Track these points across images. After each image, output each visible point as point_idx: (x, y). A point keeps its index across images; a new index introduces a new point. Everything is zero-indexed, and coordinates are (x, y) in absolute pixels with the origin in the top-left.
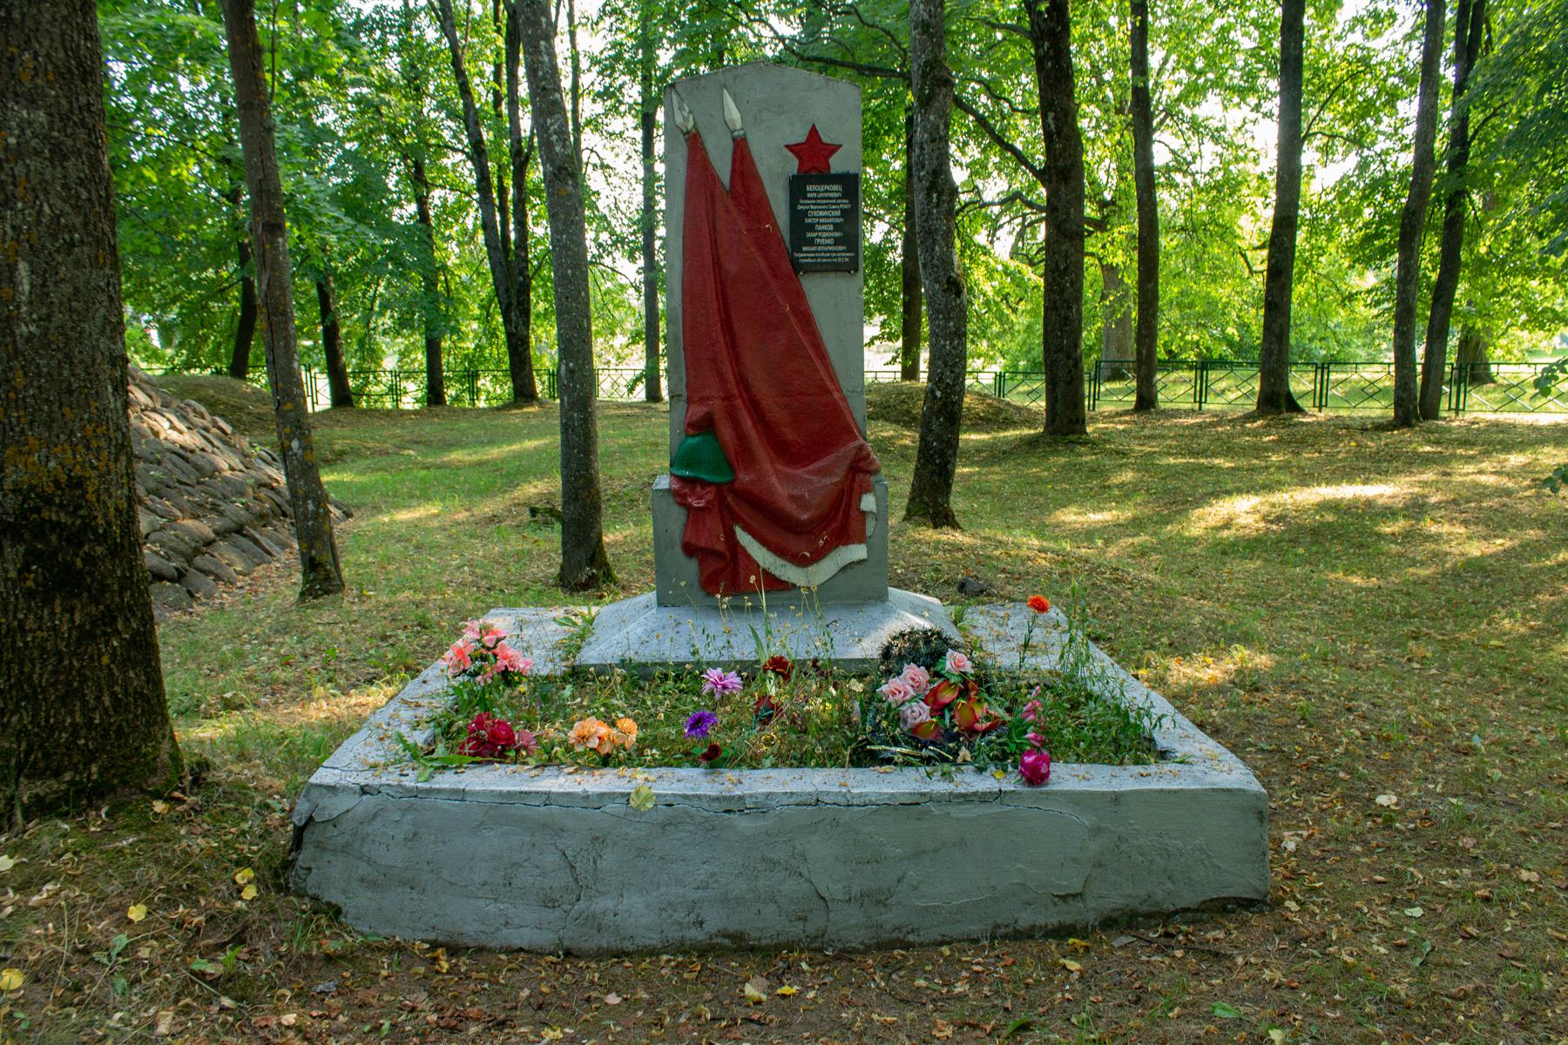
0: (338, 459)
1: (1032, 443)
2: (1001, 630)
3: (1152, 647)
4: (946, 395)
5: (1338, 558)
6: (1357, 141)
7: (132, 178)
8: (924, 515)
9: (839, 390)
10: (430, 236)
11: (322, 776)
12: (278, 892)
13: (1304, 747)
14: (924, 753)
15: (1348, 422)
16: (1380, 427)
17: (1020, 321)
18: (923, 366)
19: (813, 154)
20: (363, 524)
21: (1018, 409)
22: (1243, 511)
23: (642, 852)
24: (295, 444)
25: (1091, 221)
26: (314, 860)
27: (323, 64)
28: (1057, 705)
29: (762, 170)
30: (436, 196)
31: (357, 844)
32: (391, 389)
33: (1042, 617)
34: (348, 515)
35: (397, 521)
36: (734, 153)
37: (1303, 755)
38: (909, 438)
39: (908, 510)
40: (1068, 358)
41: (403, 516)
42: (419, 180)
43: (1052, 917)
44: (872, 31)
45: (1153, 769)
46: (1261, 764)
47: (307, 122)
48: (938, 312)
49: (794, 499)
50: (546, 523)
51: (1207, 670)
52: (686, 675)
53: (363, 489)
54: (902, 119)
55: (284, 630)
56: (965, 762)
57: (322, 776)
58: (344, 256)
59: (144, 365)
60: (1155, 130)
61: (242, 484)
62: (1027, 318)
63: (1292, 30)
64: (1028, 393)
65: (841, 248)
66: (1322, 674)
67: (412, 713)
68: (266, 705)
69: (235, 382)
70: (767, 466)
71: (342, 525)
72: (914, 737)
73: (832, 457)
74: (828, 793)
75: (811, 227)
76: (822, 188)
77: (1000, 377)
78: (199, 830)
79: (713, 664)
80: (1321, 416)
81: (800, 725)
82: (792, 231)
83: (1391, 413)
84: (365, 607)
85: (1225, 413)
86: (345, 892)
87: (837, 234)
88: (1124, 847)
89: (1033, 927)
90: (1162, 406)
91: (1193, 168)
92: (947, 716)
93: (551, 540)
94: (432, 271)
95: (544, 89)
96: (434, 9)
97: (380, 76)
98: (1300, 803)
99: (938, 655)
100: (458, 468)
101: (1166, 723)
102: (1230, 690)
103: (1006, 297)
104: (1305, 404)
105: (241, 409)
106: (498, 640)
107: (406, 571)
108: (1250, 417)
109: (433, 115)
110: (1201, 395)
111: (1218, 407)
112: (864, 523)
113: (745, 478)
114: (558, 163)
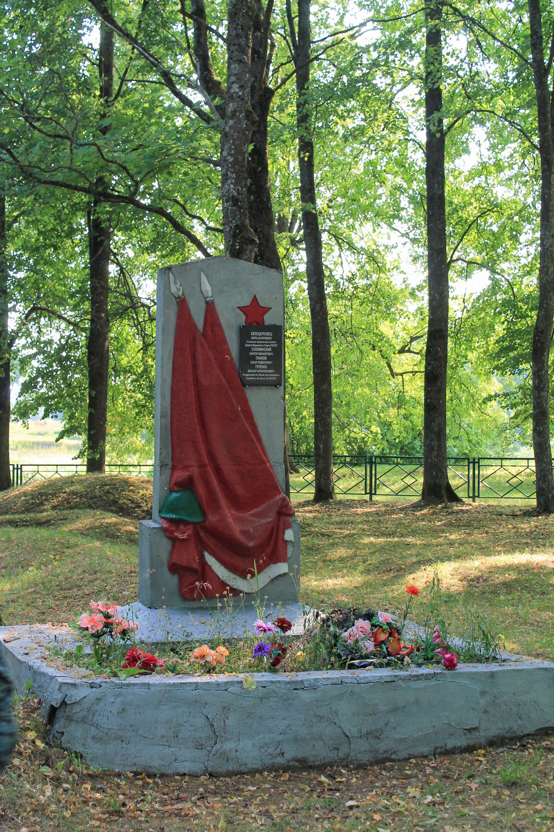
6: (490, 265)
9: (269, 462)
15: (499, 509)
16: (528, 514)
23: (249, 715)
31: (90, 716)
43: (462, 742)
49: (243, 532)
65: (271, 371)
73: (266, 505)
74: (347, 677)
76: (260, 334)
83: (534, 502)
86: (84, 745)
87: (269, 363)
88: (497, 701)
89: (454, 748)
92: (384, 647)
108: (416, 507)
113: (212, 519)
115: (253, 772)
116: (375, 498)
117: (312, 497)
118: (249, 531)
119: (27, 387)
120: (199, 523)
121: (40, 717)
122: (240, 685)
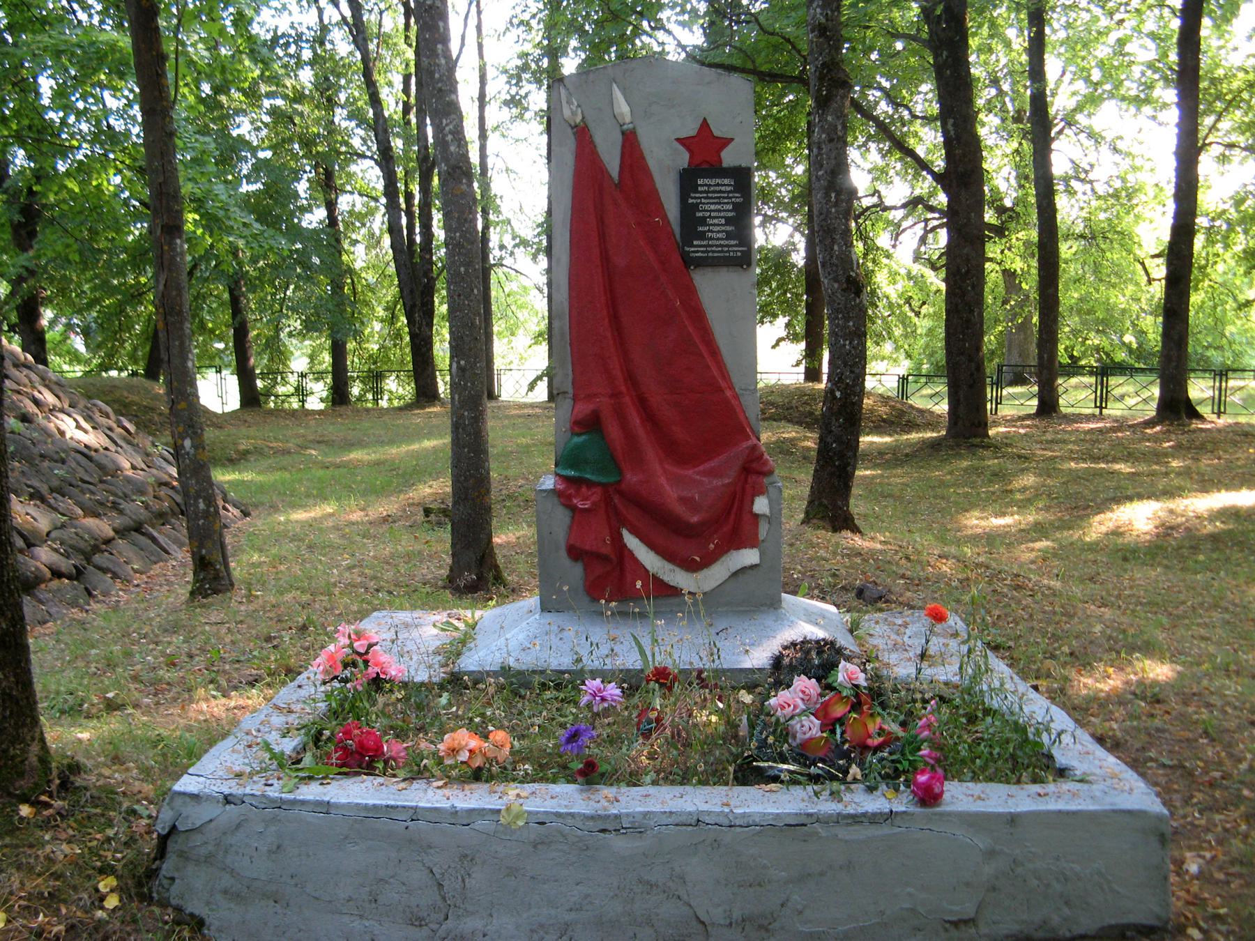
0: (235, 460)
1: (934, 446)
2: (899, 639)
3: (1053, 657)
4: (846, 395)
5: (1238, 565)
7: (56, 189)
8: (822, 518)
9: (731, 388)
10: (338, 241)
11: (187, 784)
12: (141, 902)
13: (1206, 762)
14: (813, 770)
17: (923, 325)
18: (825, 368)
19: (704, 152)
20: (259, 523)
21: (921, 411)
22: (1139, 517)
23: (512, 872)
24: (187, 443)
25: (991, 227)
26: (177, 870)
27: (239, 76)
28: (953, 719)
29: (652, 163)
30: (344, 203)
32: (297, 389)
33: (939, 628)
34: (246, 514)
35: (290, 523)
36: (623, 146)
37: (1206, 771)
38: (810, 441)
39: (807, 513)
40: (970, 360)
41: (300, 515)
42: (328, 186)
44: (775, 39)
45: (1051, 787)
46: (1163, 780)
47: (224, 133)
48: (837, 311)
49: (684, 500)
50: (439, 524)
51: (1104, 681)
52: (564, 683)
53: (261, 488)
54: (804, 125)
55: (173, 629)
56: (855, 780)
57: (187, 784)
58: (254, 261)
59: (66, 367)
60: (1053, 140)
61: (143, 482)
62: (929, 323)
63: (1189, 41)
64: (931, 396)
65: (733, 242)
66: (1223, 686)
67: (283, 719)
68: (148, 706)
69: (148, 383)
70: (656, 465)
71: (239, 524)
72: (803, 755)
73: (723, 457)
74: (709, 813)
75: (703, 221)
76: (713, 182)
77: (903, 380)
78: (63, 836)
79: (594, 674)
80: (1222, 421)
81: (681, 740)
82: (682, 225)
84: (251, 608)
85: (1125, 418)
86: (208, 903)
87: (729, 228)
88: (1019, 870)
91: (1091, 176)
92: (838, 731)
93: (441, 541)
94: (339, 273)
95: (440, 90)
96: (347, 23)
97: (294, 87)
98: (1203, 822)
99: (831, 666)
100: (355, 467)
101: (1066, 739)
102: (1130, 701)
103: (908, 301)
104: (1205, 410)
105: (153, 409)
106: (370, 646)
107: (297, 569)
108: (1150, 423)
109: (344, 124)
110: (1102, 401)
111: (1119, 413)
112: (757, 526)
114: (453, 162)
117: (1033, 411)
118: (693, 498)
120: (612, 485)
122: (495, 817)
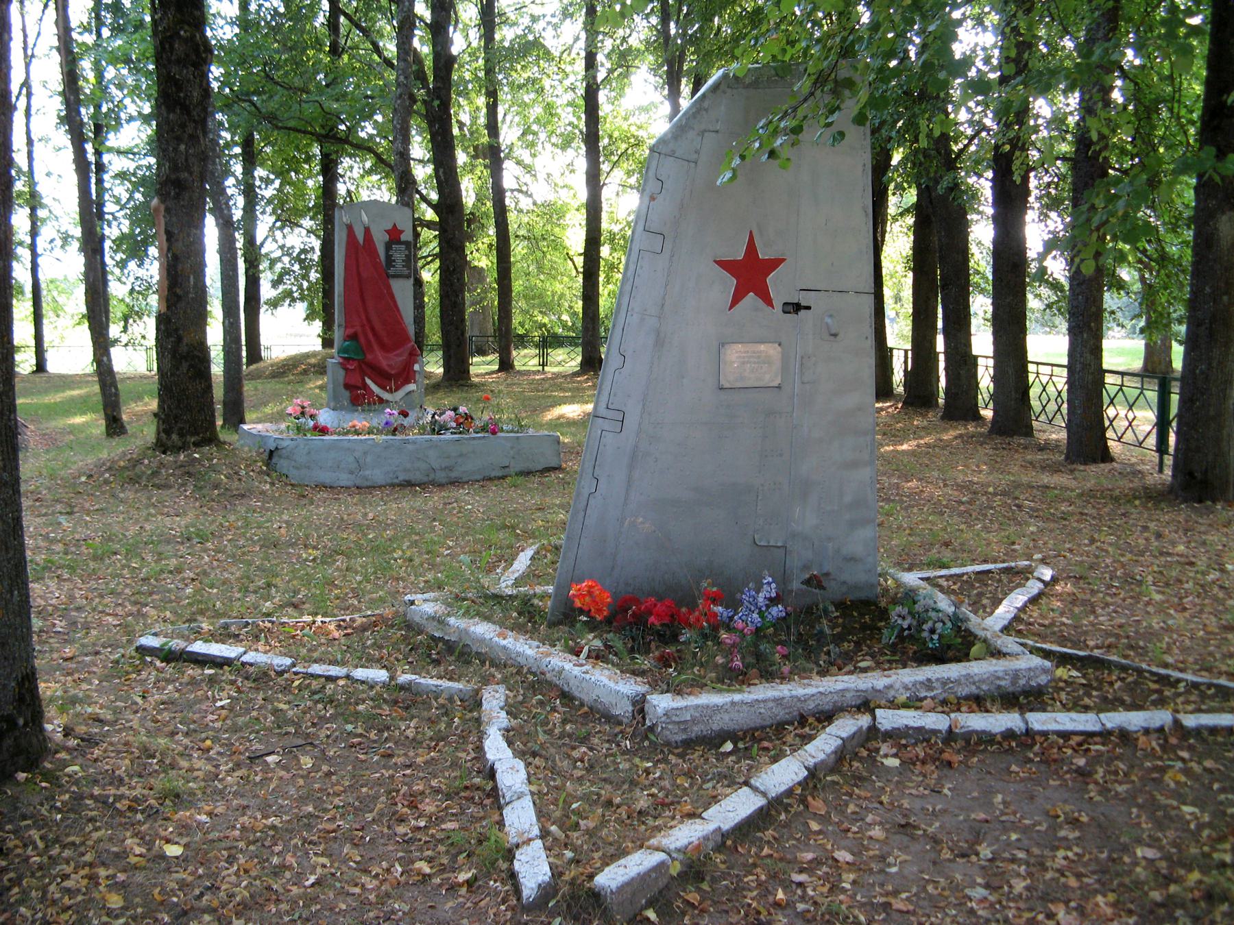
90: (517, 368)
108: (575, 374)
113: (370, 357)
115: (380, 487)
116: (546, 368)
119: (275, 284)
121: (265, 456)
